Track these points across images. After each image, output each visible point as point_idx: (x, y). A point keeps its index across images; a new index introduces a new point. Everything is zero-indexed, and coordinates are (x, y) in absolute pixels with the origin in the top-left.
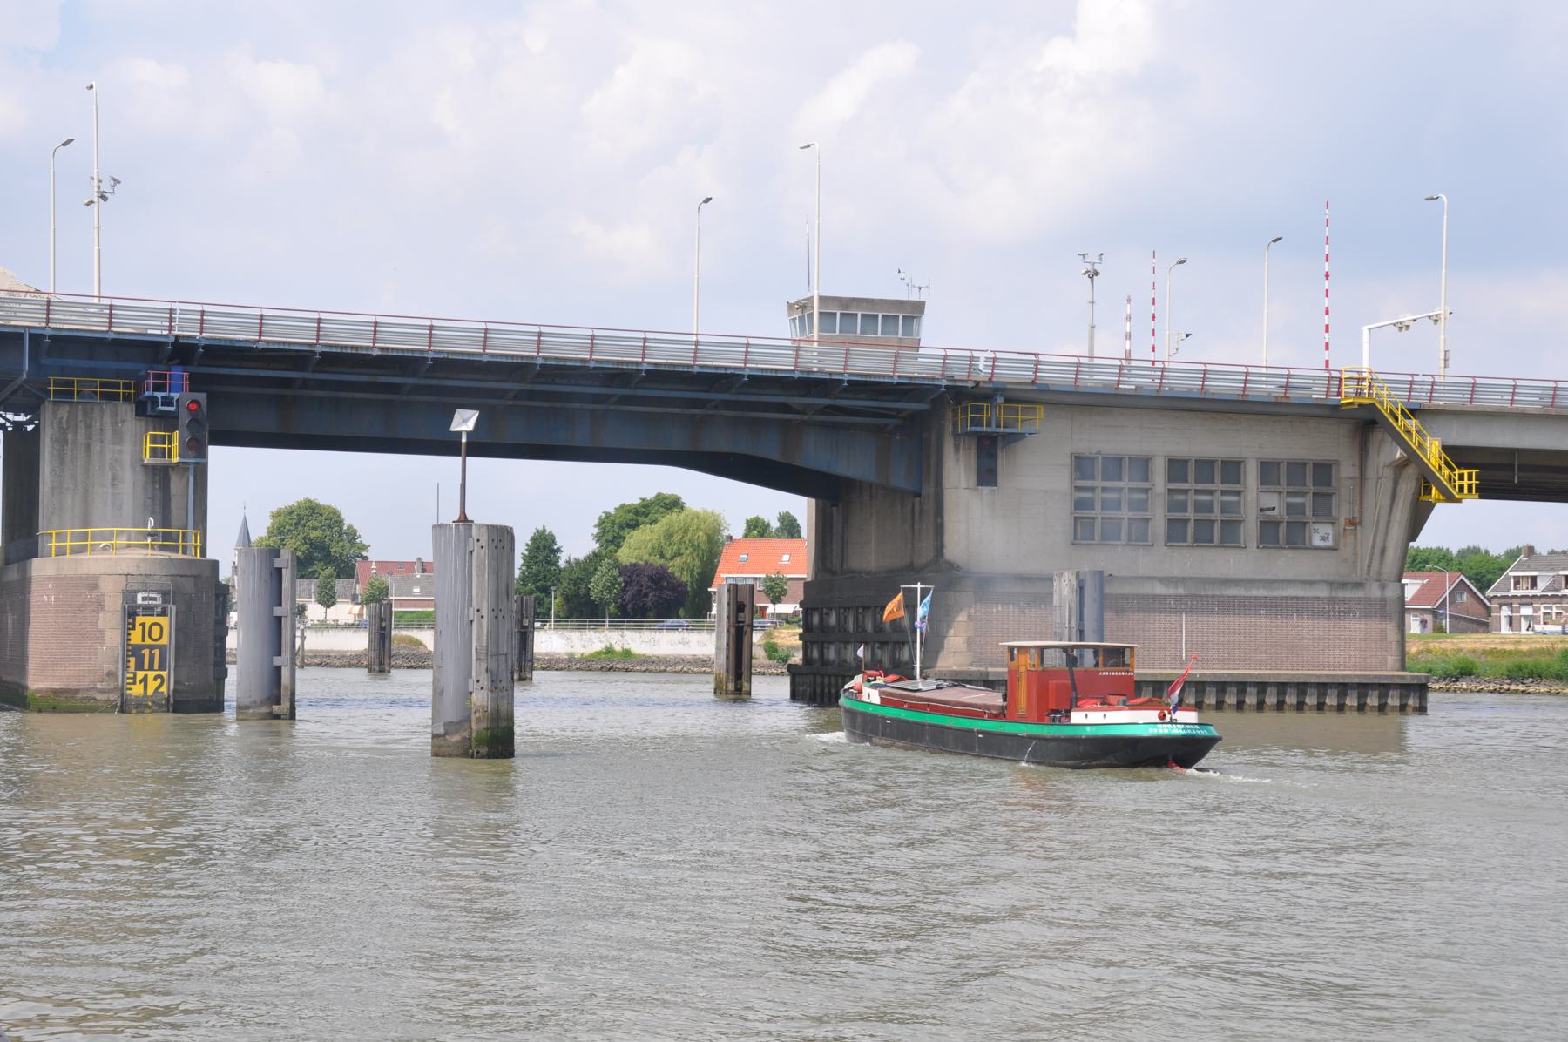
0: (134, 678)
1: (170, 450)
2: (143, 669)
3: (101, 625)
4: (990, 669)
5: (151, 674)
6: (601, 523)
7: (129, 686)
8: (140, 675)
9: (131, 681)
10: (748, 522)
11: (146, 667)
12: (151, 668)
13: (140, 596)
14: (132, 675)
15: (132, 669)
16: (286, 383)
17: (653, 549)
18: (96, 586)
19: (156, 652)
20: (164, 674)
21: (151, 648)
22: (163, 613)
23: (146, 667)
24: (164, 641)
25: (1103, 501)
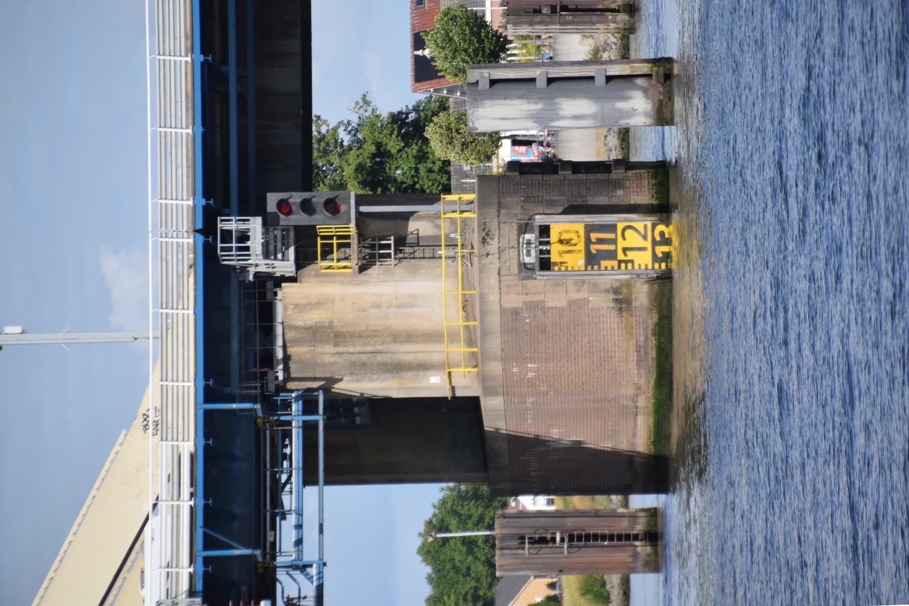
0: (626, 262)
1: (339, 237)
2: (615, 251)
3: (563, 303)
4: (474, 9)
5: (621, 244)
6: (426, 578)
7: (636, 267)
8: (621, 256)
9: (630, 265)
10: (418, 553)
11: (612, 247)
12: (614, 241)
13: (527, 260)
14: (623, 265)
15: (615, 263)
16: (241, 99)
17: (434, 601)
18: (516, 312)
19: (594, 236)
20: (620, 226)
21: (588, 241)
22: (545, 231)
23: (612, 247)
24: (581, 228)
25: (380, 254)
